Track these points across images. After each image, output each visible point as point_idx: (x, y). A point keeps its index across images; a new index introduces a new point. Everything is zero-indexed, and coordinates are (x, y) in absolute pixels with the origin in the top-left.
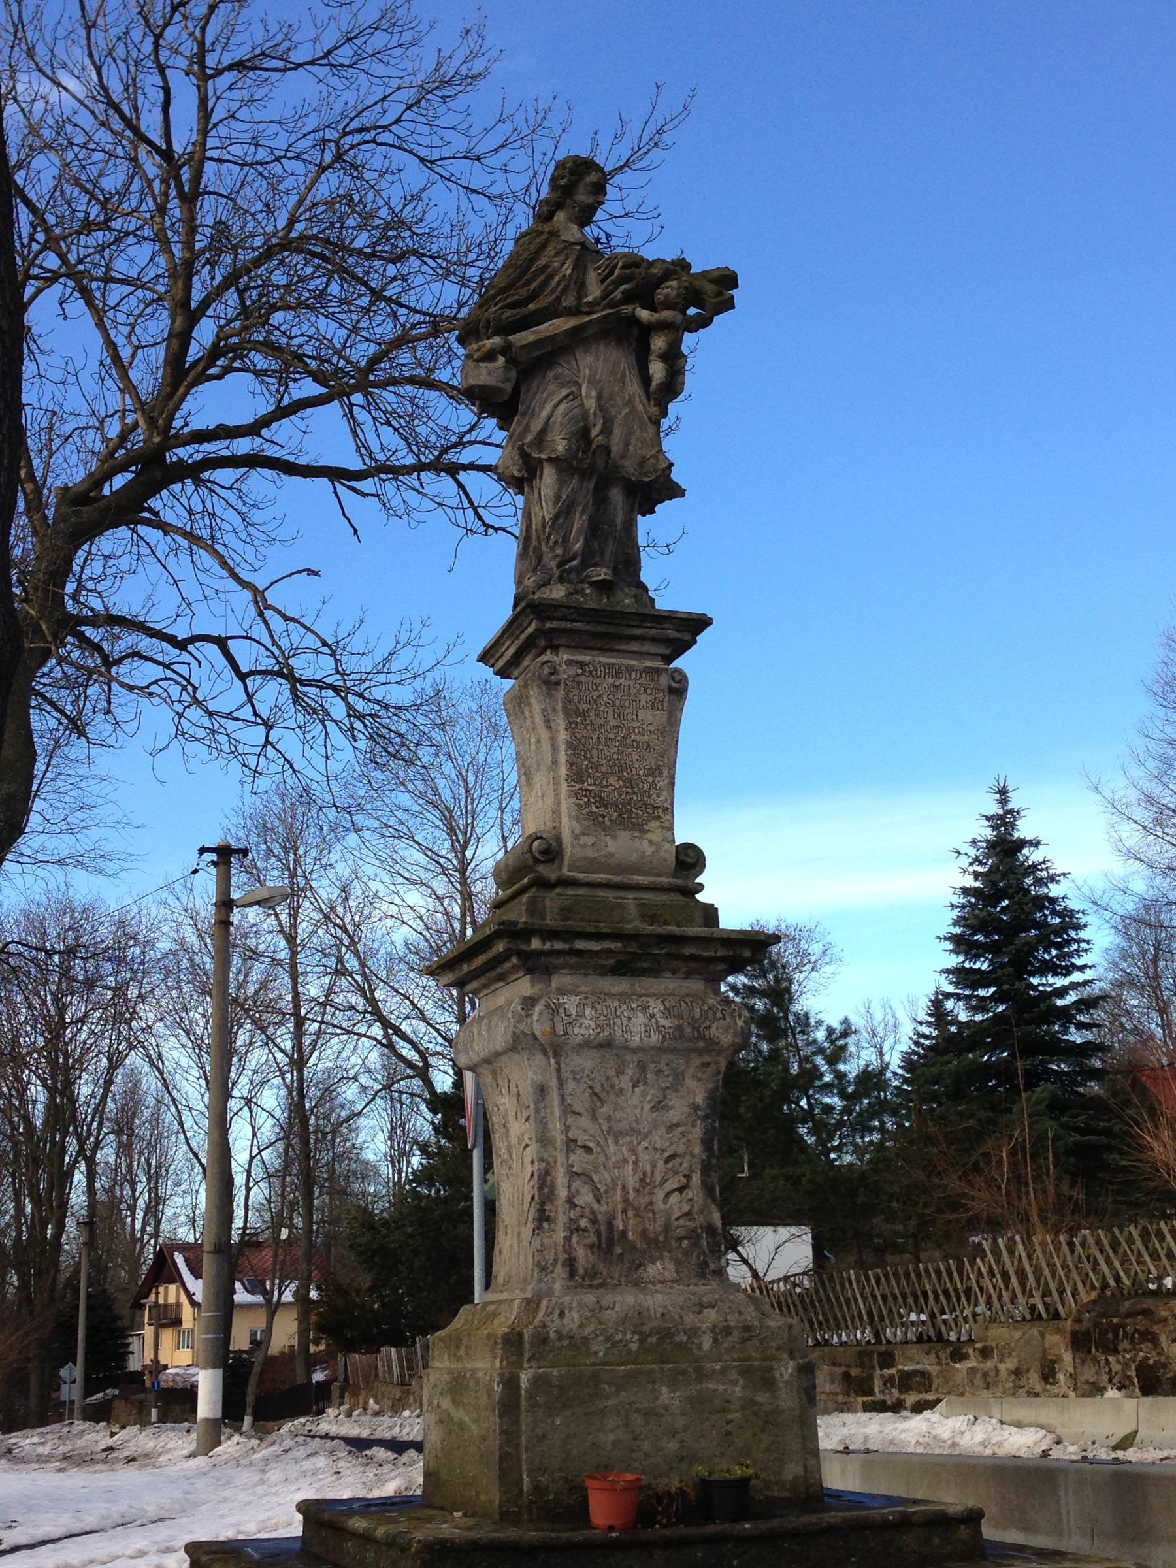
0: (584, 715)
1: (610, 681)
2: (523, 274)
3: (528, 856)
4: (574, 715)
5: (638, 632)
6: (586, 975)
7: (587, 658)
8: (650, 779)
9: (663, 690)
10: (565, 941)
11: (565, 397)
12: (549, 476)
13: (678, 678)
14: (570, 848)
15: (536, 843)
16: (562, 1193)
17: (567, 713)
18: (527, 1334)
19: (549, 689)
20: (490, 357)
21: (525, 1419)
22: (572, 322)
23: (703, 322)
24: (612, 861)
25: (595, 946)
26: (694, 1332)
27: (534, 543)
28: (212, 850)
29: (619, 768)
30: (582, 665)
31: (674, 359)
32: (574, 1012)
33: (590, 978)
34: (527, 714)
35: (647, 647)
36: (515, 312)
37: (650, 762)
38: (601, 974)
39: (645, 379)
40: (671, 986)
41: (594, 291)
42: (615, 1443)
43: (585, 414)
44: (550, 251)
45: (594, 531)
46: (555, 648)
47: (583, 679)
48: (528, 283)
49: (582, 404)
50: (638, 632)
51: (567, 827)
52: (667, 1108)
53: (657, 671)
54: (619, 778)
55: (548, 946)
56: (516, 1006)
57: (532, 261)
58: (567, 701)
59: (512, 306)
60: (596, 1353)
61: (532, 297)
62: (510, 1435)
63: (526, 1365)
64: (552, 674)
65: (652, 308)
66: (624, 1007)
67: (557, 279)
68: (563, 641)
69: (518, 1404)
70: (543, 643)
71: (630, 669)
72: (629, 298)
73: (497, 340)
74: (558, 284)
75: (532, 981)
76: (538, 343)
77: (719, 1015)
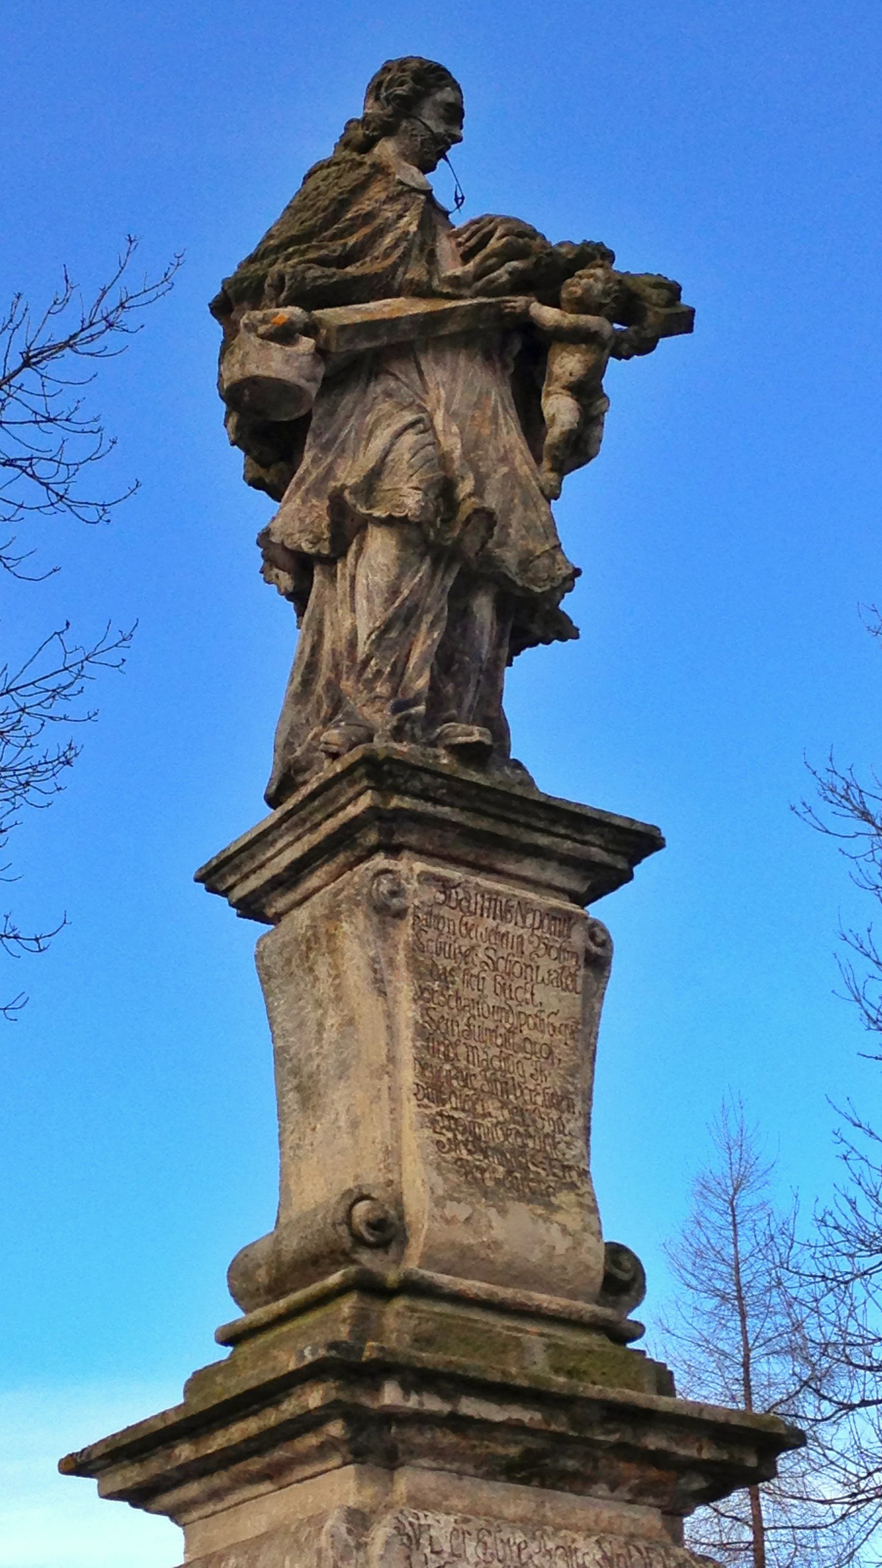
0: (445, 977)
1: (491, 923)
3: (343, 1230)
4: (430, 976)
5: (543, 841)
6: (460, 1474)
8: (554, 1114)
9: (575, 954)
10: (445, 1396)
11: (412, 425)
12: (379, 551)
13: (601, 937)
15: (361, 1208)
17: (414, 965)
19: (383, 922)
22: (421, 307)
24: (500, 1258)
25: (495, 1413)
27: (325, 672)
29: (504, 1087)
30: (445, 885)
32: (447, 1548)
33: (467, 1482)
34: (322, 970)
35: (553, 874)
37: (554, 1082)
38: (490, 1476)
39: (532, 422)
40: (606, 1514)
43: (444, 460)
45: (445, 661)
46: (394, 851)
47: (445, 911)
49: (436, 443)
50: (543, 841)
53: (568, 918)
54: (504, 1105)
55: (412, 1402)
56: (334, 1522)
57: (343, 204)
58: (416, 948)
59: (322, 262)
61: (344, 260)
64: (393, 894)
66: (534, 1547)
67: (388, 240)
68: (413, 839)
70: (372, 838)
71: (525, 907)
72: (521, 284)
74: (395, 246)
75: (360, 1475)
76: (370, 328)
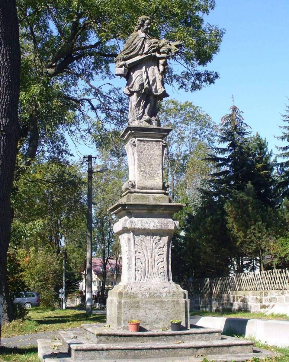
2: (130, 46)
8: (157, 167)
15: (129, 183)
16: (134, 263)
17: (137, 152)
18: (124, 292)
20: (121, 67)
21: (123, 310)
26: (161, 293)
36: (127, 55)
41: (147, 49)
42: (142, 316)
44: (136, 40)
48: (131, 48)
57: (132, 42)
60: (139, 297)
62: (119, 313)
63: (123, 299)
65: (160, 53)
69: (121, 306)
73: (123, 63)
77: (171, 223)
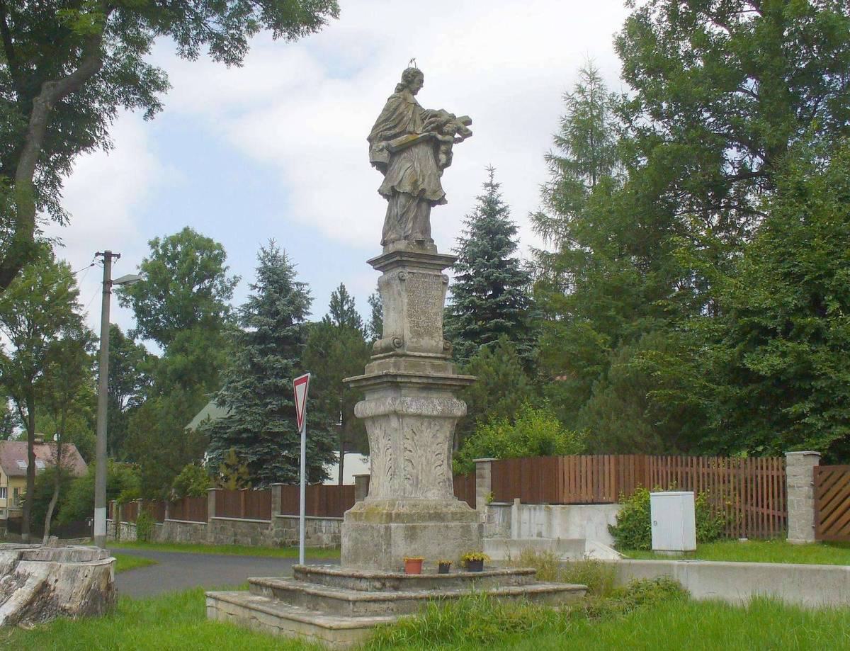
0: (413, 292)
7: (415, 271)
14: (408, 343)
23: (460, 140)
28: (103, 254)
30: (413, 273)
31: (449, 154)
51: (407, 335)
52: (437, 437)
72: (433, 129)
